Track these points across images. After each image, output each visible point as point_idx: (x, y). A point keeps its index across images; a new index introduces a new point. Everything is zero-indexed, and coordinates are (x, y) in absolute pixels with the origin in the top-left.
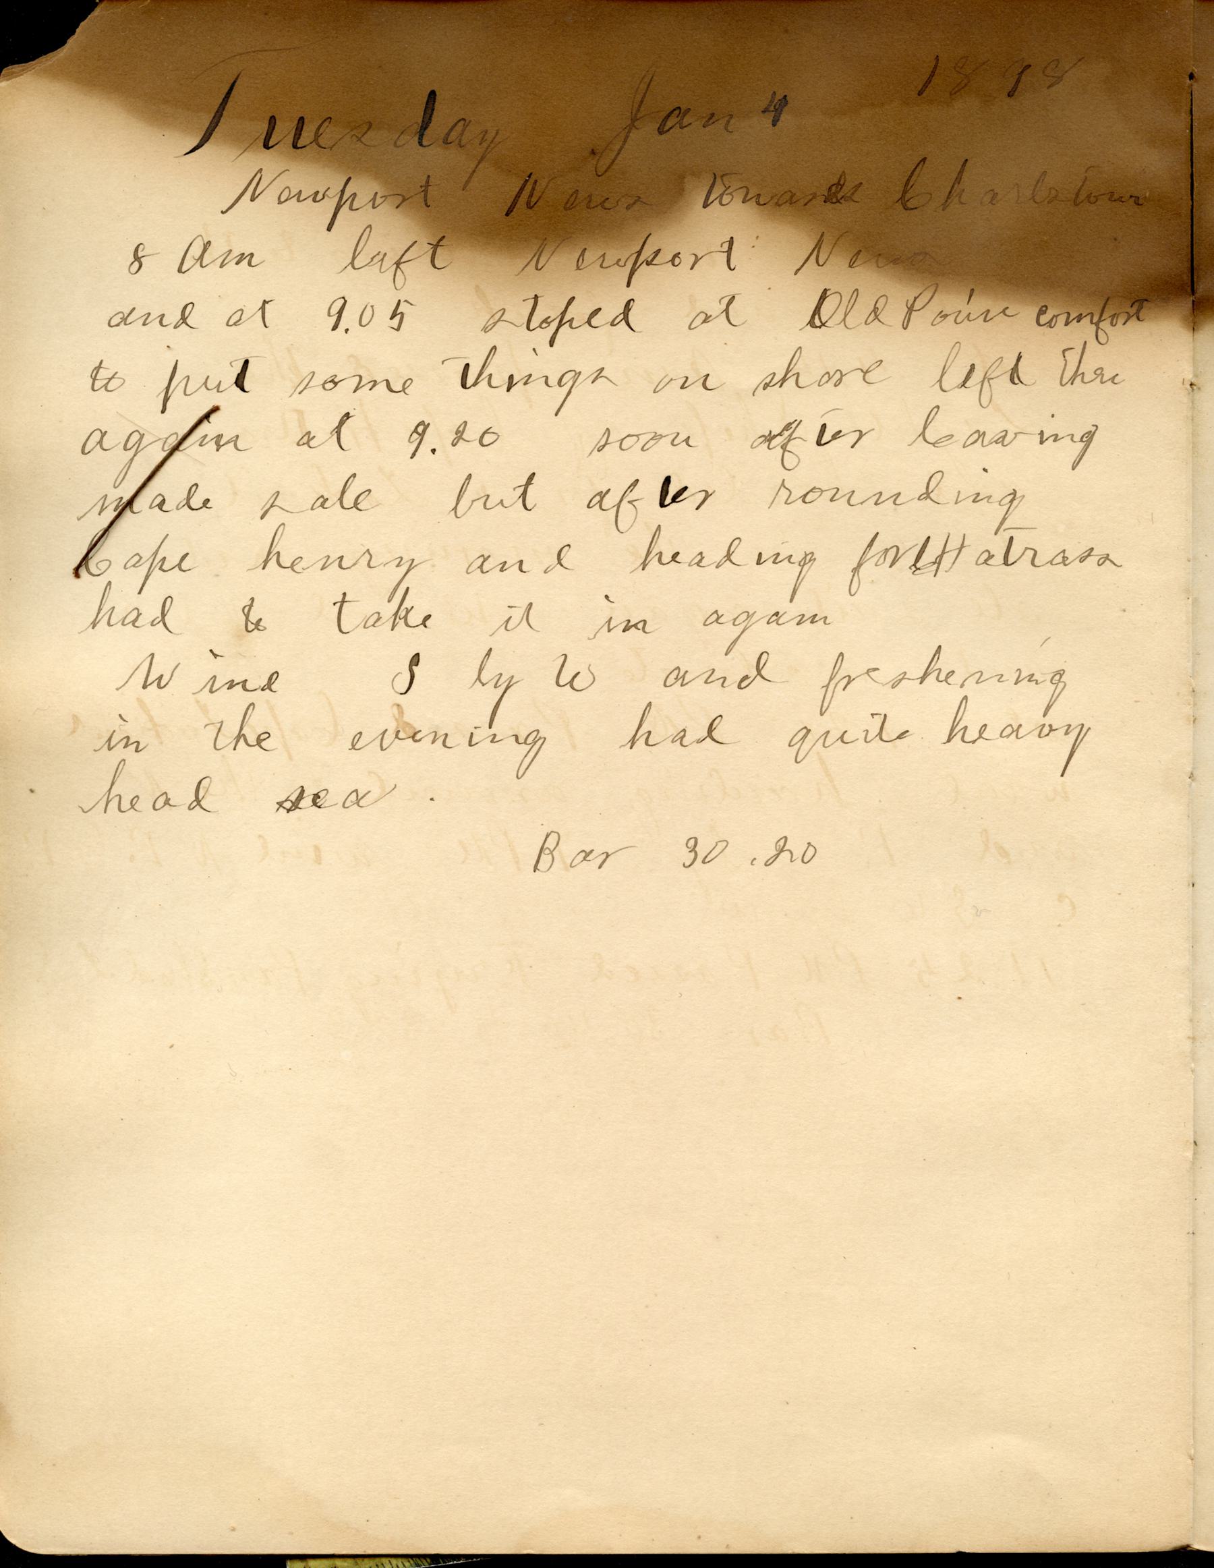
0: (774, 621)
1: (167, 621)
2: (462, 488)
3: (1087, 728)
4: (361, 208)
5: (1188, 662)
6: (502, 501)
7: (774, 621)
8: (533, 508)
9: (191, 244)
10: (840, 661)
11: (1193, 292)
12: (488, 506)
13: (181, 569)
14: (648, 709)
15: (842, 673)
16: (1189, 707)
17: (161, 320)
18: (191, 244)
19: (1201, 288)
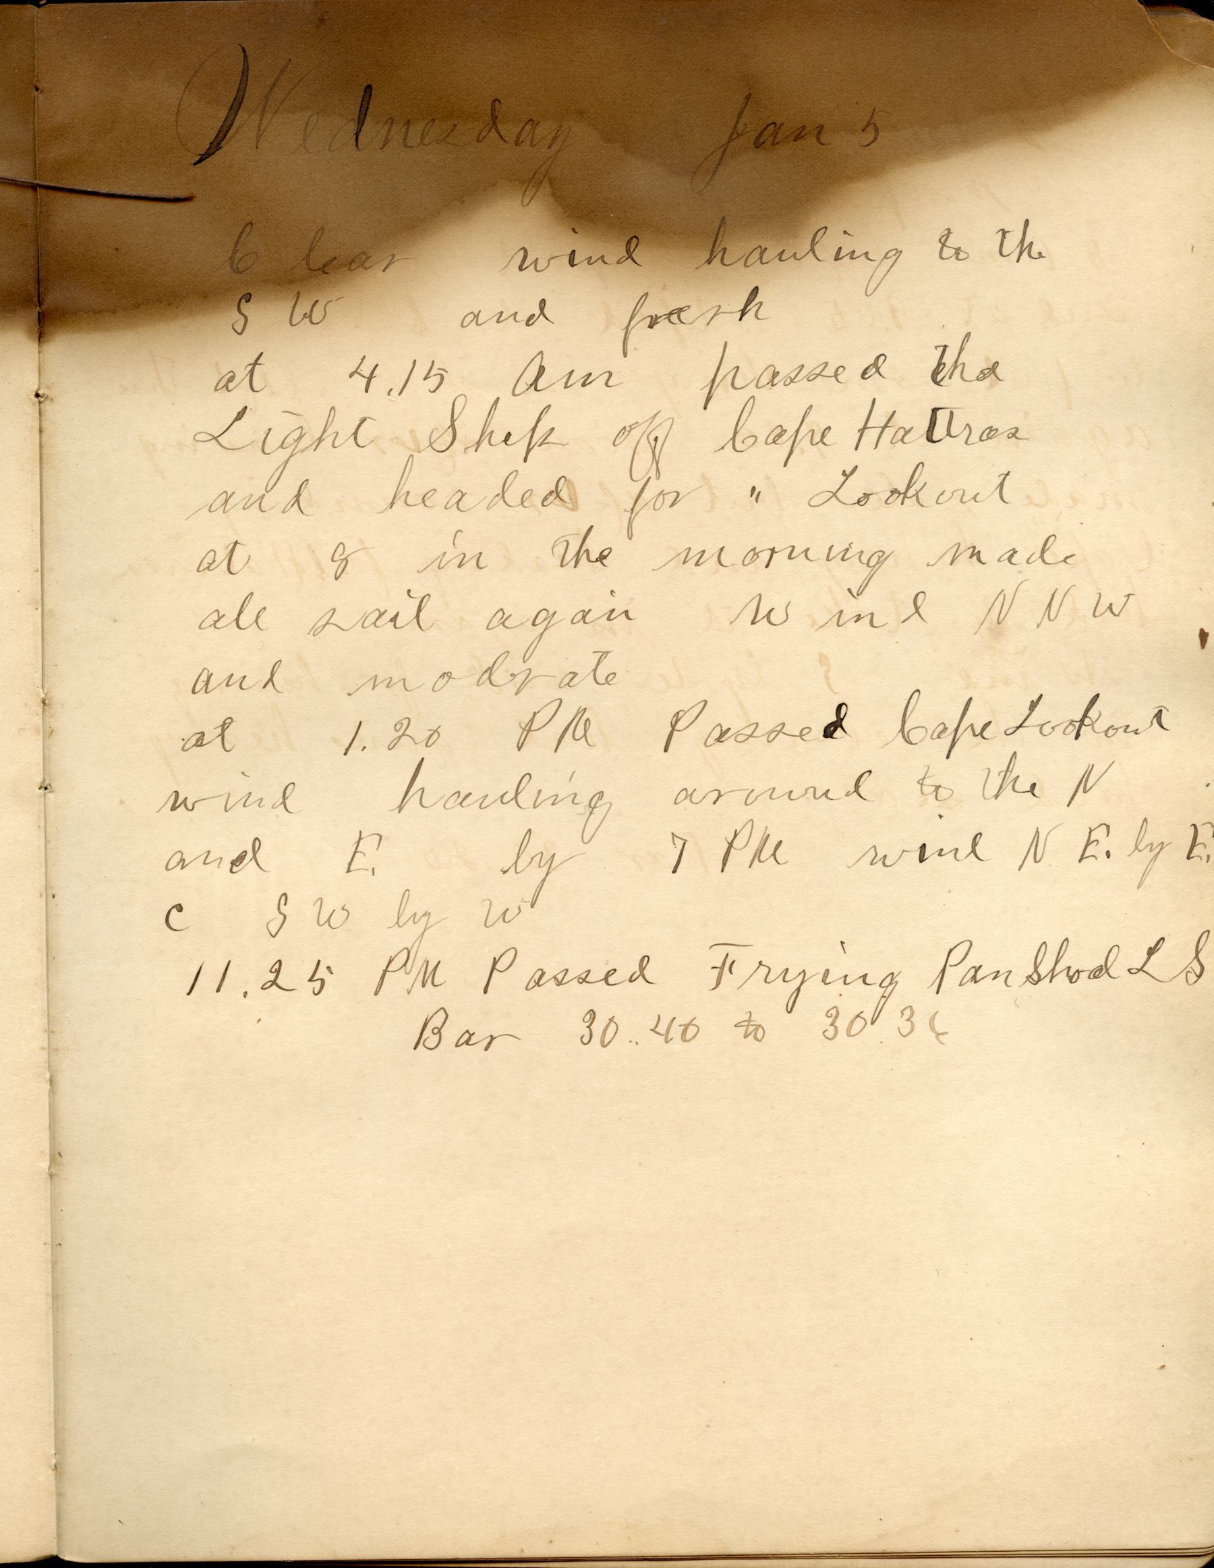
1: (546, 313)
4: (1012, 252)
5: (36, 672)
10: (643, 300)
11: (40, 303)
14: (249, 597)
16: (38, 717)
19: (49, 301)
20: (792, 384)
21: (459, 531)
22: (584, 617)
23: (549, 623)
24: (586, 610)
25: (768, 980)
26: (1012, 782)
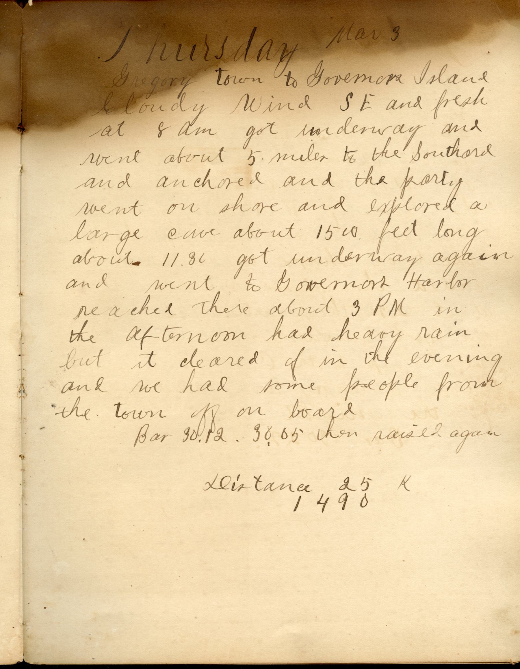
0: (417, 105)
2: (238, 274)
3: (383, 156)
6: (312, 180)
7: (417, 105)
8: (434, 338)
9: (131, 412)
12: (141, 367)
13: (140, 418)
15: (445, 99)
17: (292, 157)
18: (131, 412)
20: (316, 78)
21: (328, 240)
22: (292, 181)
23: (396, 306)
24: (479, 431)
25: (462, 390)
26: (248, 260)
